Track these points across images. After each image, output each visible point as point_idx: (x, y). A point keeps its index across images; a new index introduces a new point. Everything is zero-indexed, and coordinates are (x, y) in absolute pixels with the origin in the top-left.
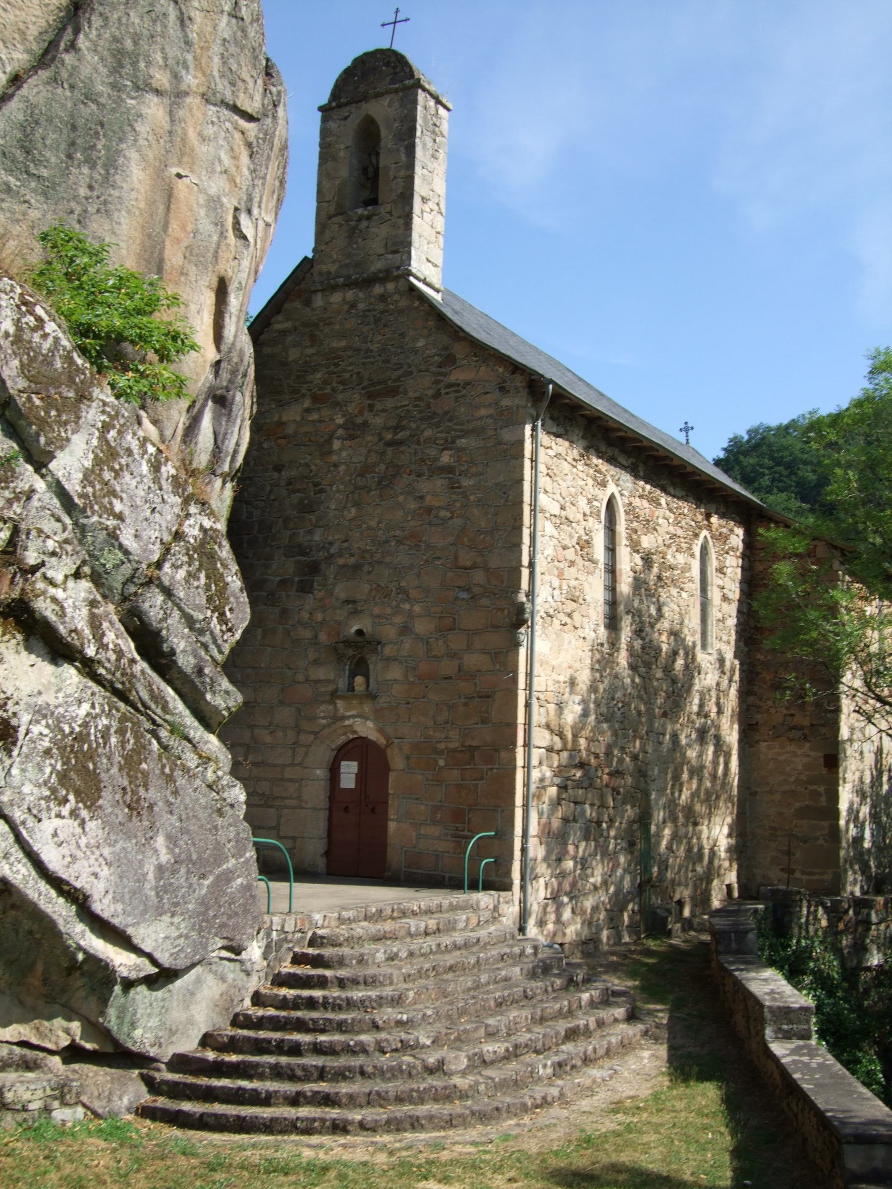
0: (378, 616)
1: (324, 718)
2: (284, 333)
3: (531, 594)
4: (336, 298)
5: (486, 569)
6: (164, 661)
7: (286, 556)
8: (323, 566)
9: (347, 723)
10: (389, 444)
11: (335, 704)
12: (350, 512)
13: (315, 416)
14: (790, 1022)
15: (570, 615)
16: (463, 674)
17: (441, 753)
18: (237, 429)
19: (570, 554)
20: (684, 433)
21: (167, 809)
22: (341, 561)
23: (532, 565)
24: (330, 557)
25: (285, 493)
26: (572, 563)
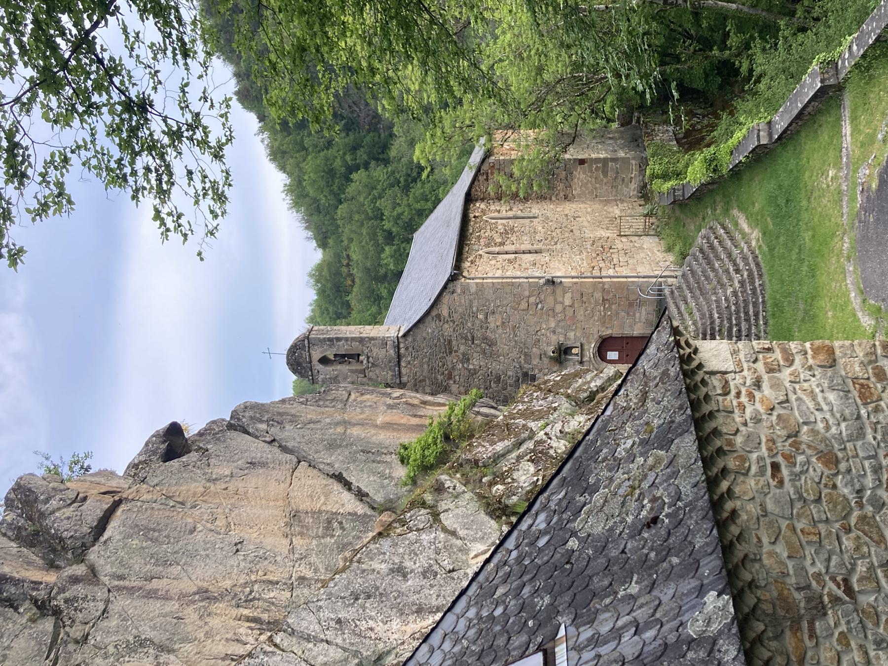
3: (540, 278)
4: (404, 371)
5: (529, 297)
10: (473, 343)
17: (605, 314)
19: (516, 266)
22: (523, 362)
23: (527, 278)
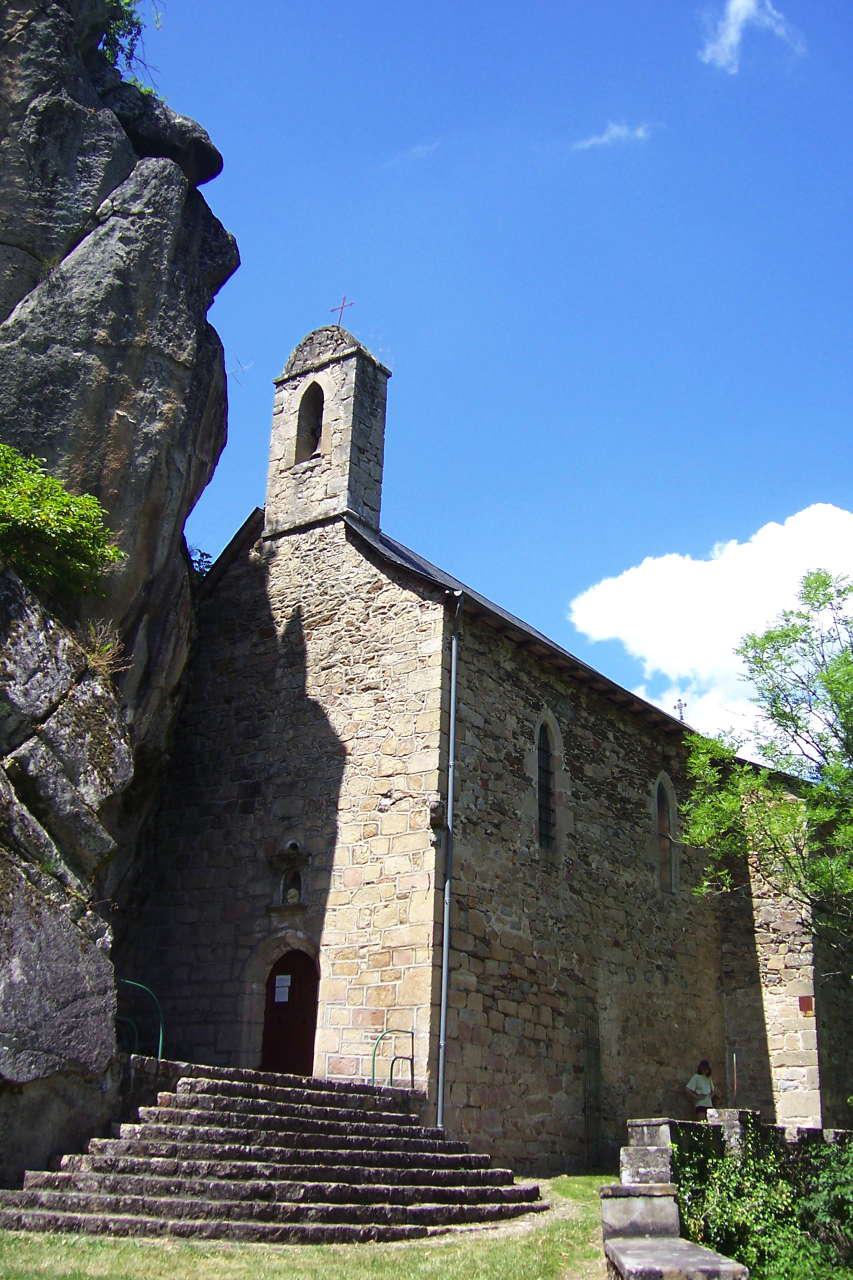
0: (310, 829)
1: (260, 932)
2: (238, 578)
6: (41, 806)
7: (232, 780)
8: (263, 788)
9: (280, 935)
11: (270, 916)
12: (288, 733)
13: (262, 649)
14: (647, 1165)
15: (497, 826)
16: (383, 878)
18: (171, 647)
19: (497, 768)
20: (678, 710)
21: (27, 936)
22: (279, 781)
24: (269, 779)
25: (234, 721)
26: (499, 777)
